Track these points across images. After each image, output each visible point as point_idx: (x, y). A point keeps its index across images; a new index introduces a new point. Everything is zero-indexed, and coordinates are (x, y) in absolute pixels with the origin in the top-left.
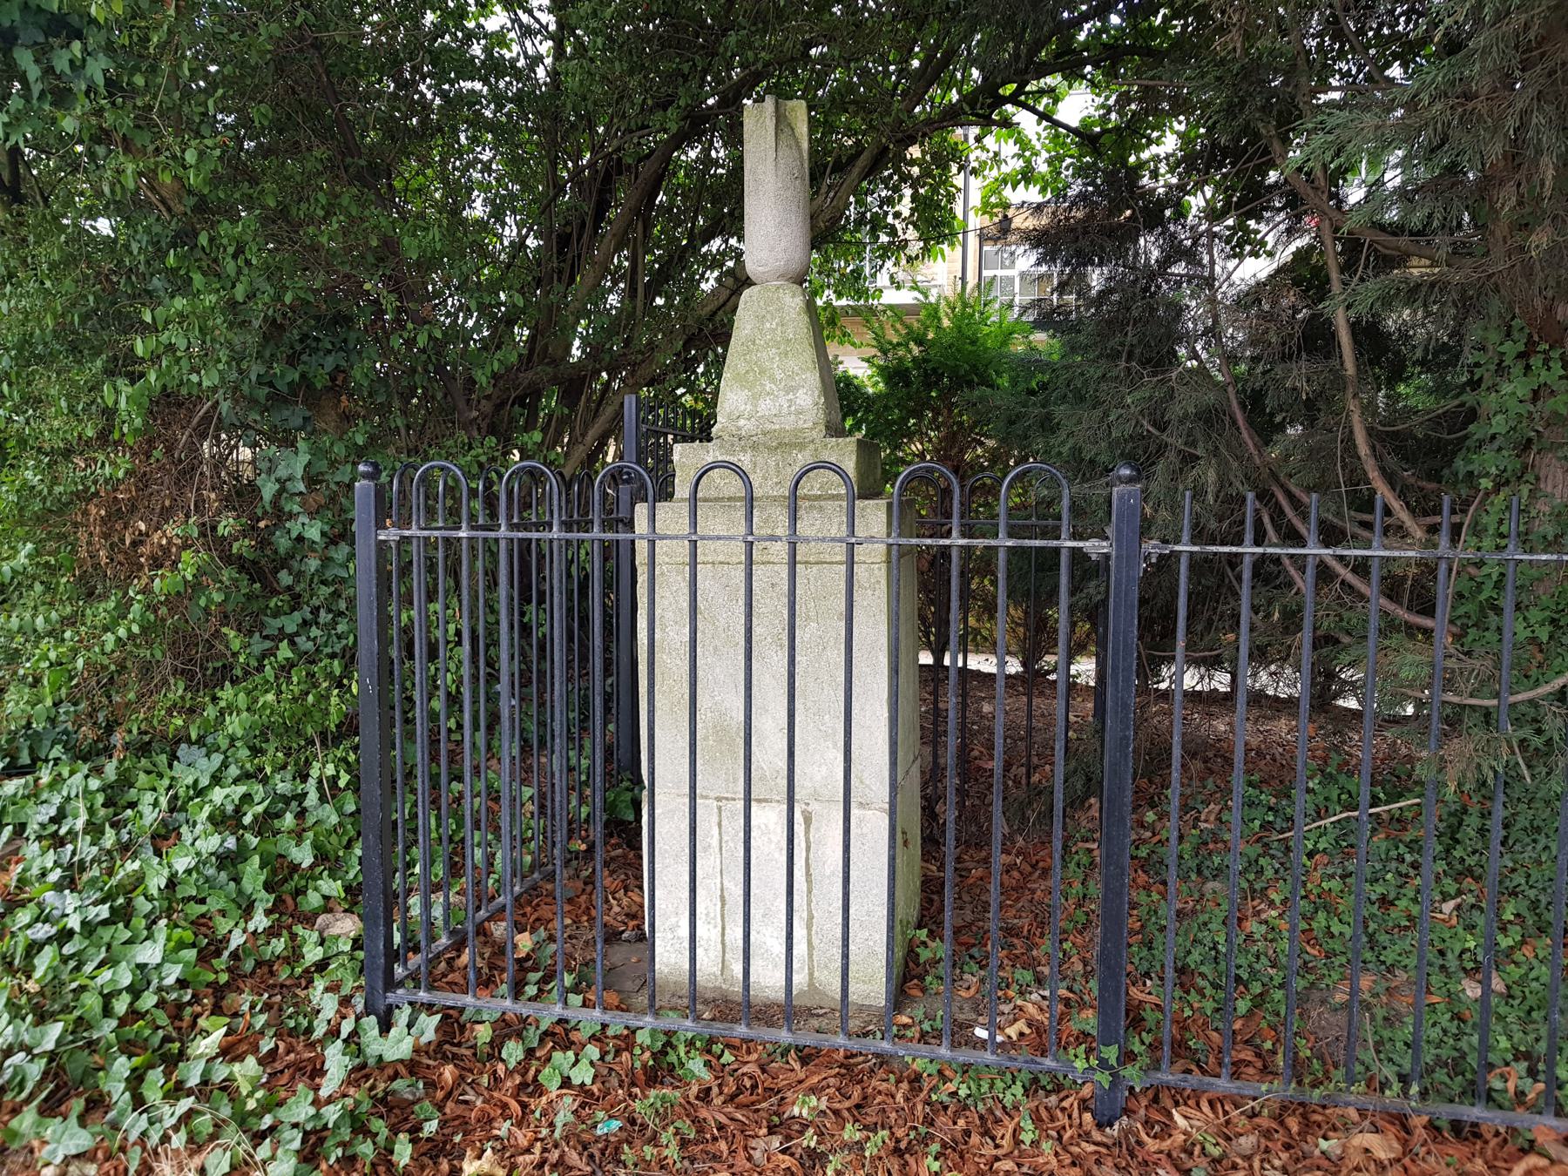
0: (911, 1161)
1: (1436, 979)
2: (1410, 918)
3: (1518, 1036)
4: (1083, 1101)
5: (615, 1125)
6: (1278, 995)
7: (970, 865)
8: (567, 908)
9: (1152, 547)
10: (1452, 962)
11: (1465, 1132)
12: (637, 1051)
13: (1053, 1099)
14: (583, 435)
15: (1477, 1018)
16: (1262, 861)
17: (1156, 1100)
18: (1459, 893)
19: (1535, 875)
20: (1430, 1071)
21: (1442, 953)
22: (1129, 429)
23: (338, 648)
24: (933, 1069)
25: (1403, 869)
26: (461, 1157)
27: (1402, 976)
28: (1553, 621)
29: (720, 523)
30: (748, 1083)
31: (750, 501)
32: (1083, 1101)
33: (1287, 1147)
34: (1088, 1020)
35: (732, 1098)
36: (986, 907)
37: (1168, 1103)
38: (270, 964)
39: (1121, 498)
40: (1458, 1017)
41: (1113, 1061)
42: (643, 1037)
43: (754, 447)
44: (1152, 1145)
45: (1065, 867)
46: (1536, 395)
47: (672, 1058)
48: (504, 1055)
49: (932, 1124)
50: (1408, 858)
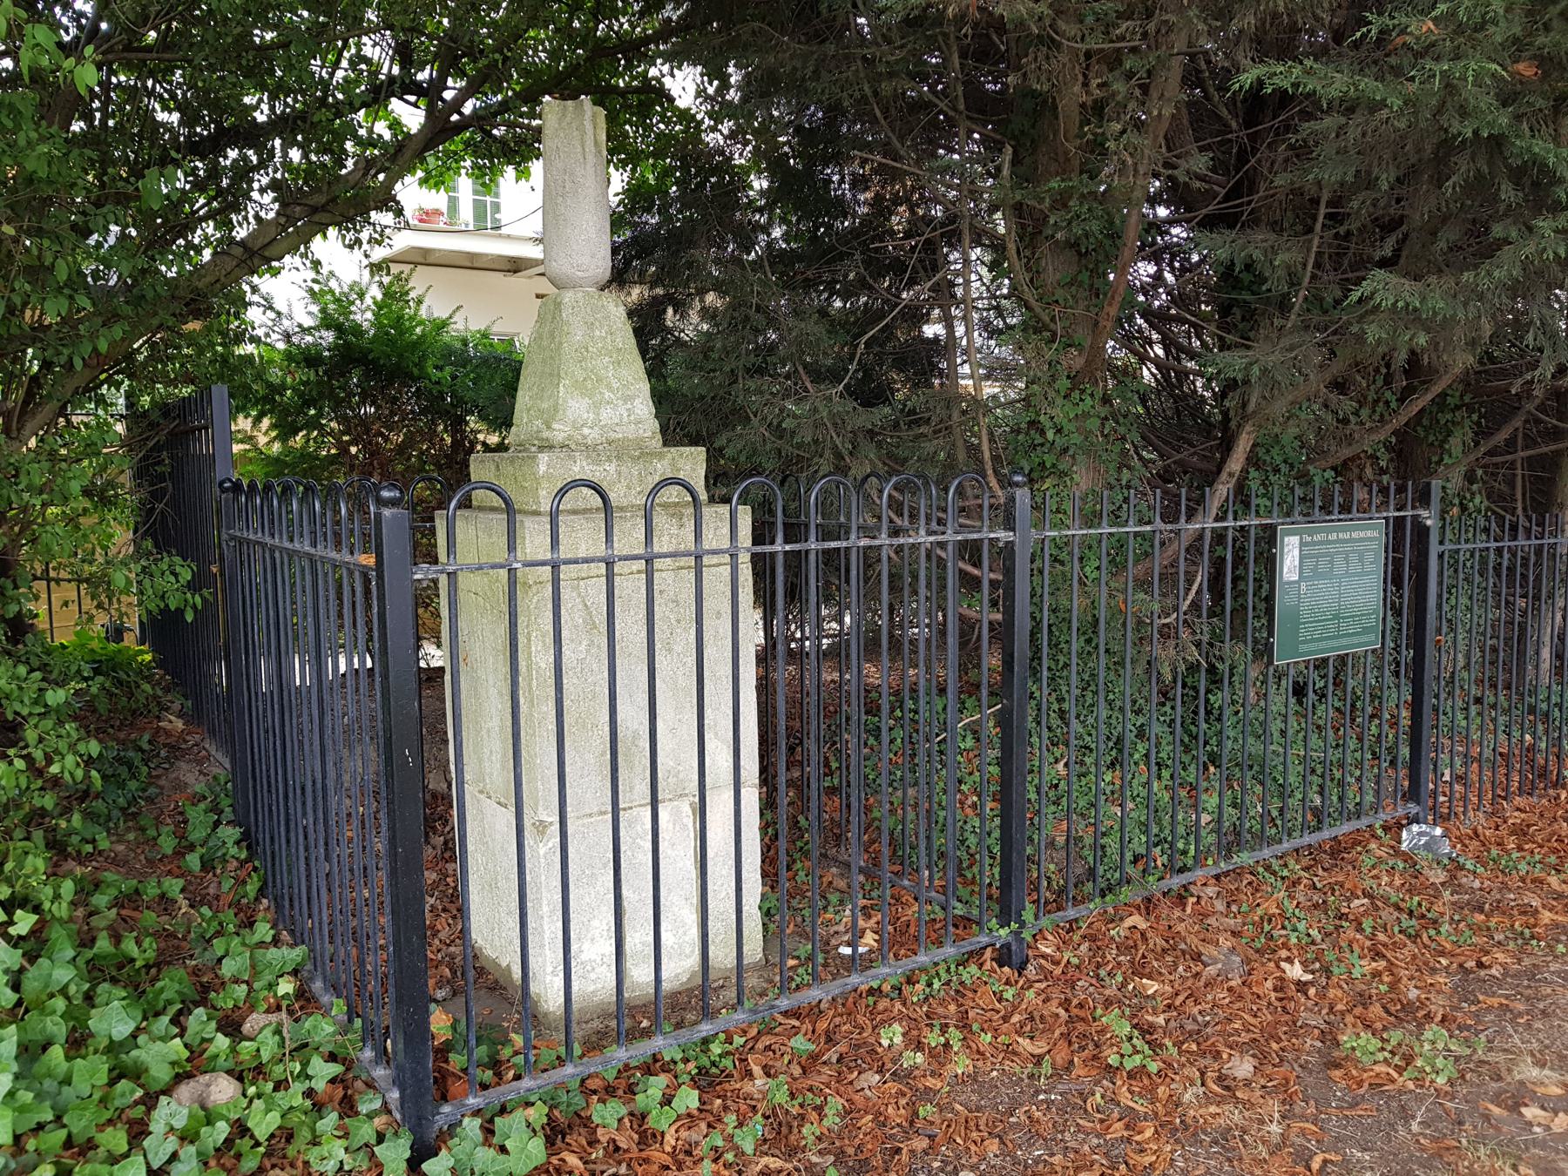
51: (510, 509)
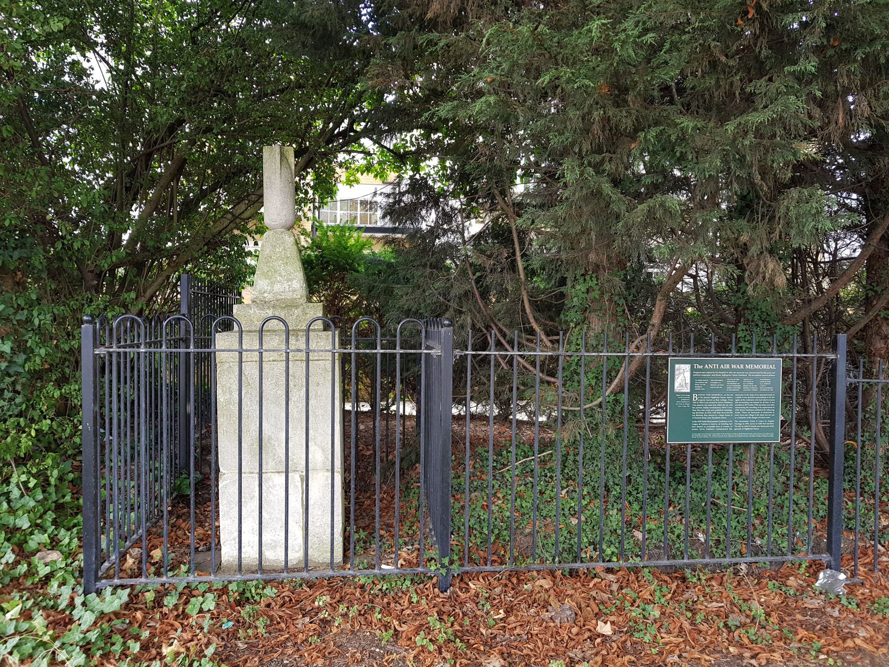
0: (369, 616)
1: (561, 519)
2: (551, 498)
3: (590, 536)
4: (434, 585)
5: (231, 624)
6: (505, 533)
7: (363, 500)
9: (458, 352)
10: (567, 512)
11: (573, 573)
12: (231, 593)
13: (422, 585)
14: (145, 292)
15: (577, 532)
17: (462, 580)
18: (568, 486)
19: (593, 476)
20: (561, 554)
21: (563, 509)
22: (435, 300)
23: (16, 412)
24: (370, 581)
25: (547, 479)
26: (160, 647)
27: (549, 520)
28: (596, 377)
29: (252, 342)
30: (287, 599)
32: (434, 585)
33: (513, 589)
34: (434, 553)
35: (282, 606)
36: (374, 517)
37: (467, 580)
38: (17, 579)
40: (570, 532)
41: (447, 564)
42: (233, 587)
44: (463, 596)
46: (588, 291)
47: (248, 595)
48: (166, 603)
49: (372, 602)
50: (549, 475)
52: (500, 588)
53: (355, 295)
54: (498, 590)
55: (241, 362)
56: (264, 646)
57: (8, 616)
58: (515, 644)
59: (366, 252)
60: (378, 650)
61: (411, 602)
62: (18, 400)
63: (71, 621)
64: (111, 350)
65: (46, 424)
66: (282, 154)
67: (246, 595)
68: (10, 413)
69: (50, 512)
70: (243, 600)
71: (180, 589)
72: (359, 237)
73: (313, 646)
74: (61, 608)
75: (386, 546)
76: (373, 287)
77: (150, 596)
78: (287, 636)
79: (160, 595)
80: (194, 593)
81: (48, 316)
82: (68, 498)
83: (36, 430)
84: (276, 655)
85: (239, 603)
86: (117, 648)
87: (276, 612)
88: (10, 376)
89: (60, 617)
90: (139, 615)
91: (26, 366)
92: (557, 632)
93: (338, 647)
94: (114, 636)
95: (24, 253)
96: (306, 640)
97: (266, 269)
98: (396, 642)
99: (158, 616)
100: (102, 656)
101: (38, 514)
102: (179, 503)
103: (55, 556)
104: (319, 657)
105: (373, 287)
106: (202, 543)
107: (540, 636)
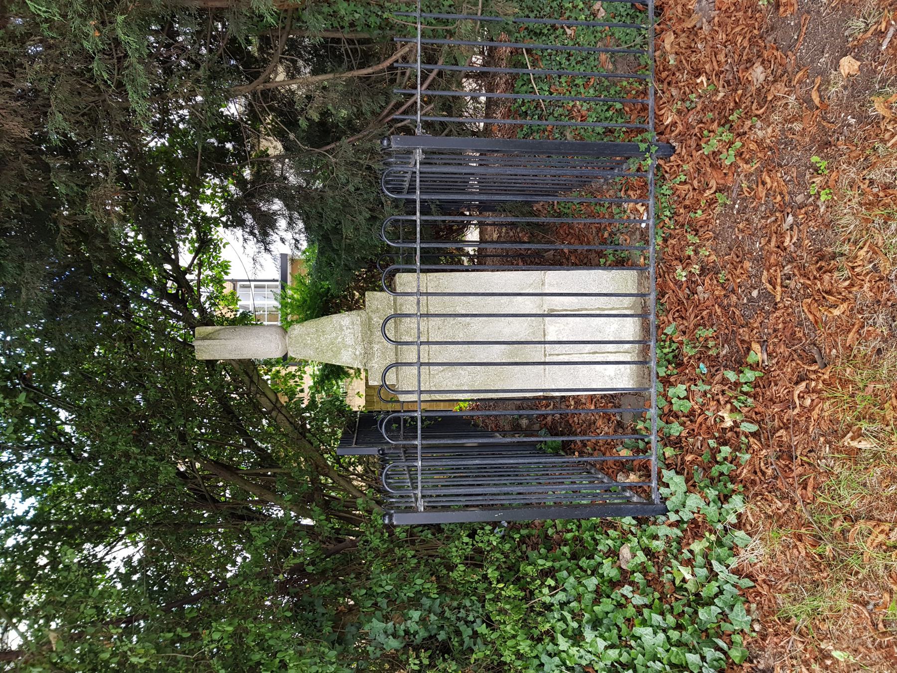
5: (702, 365)
8: (608, 454)
12: (669, 372)
16: (556, 115)
18: (562, 27)
23: (479, 605)
31: (397, 364)
33: (674, 74)
37: (663, 127)
39: (397, 144)
43: (370, 343)
44: (680, 127)
45: (567, 215)
48: (678, 434)
51: (397, 364)
52: (673, 90)
53: (354, 294)
54: (674, 92)
55: (428, 343)
56: (727, 328)
57: (688, 577)
58: (736, 57)
59: (308, 281)
60: (737, 206)
61: (685, 183)
62: (468, 603)
63: (694, 521)
64: (420, 495)
65: (492, 573)
66: (204, 338)
67: (671, 358)
68: (480, 610)
69: (580, 563)
70: (677, 361)
71: (663, 424)
72: (292, 289)
73: (729, 276)
74: (680, 534)
75: (621, 227)
76: (345, 265)
77: (669, 452)
78: (716, 306)
79: (666, 440)
80: (666, 410)
81: (382, 577)
82: (566, 549)
83: (498, 582)
84: (737, 313)
85: (680, 365)
86: (725, 468)
87: (693, 321)
88: (443, 612)
89: (689, 533)
90: (689, 458)
91: (433, 596)
92: (726, 11)
93: (731, 250)
94: (712, 474)
95: (319, 602)
96: (722, 285)
97: (330, 354)
98: (729, 188)
99: (691, 440)
100: (733, 482)
101: (582, 574)
102: (570, 449)
103: (625, 552)
104: (742, 267)
105: (345, 265)
106: (613, 418)
107: (729, 29)
